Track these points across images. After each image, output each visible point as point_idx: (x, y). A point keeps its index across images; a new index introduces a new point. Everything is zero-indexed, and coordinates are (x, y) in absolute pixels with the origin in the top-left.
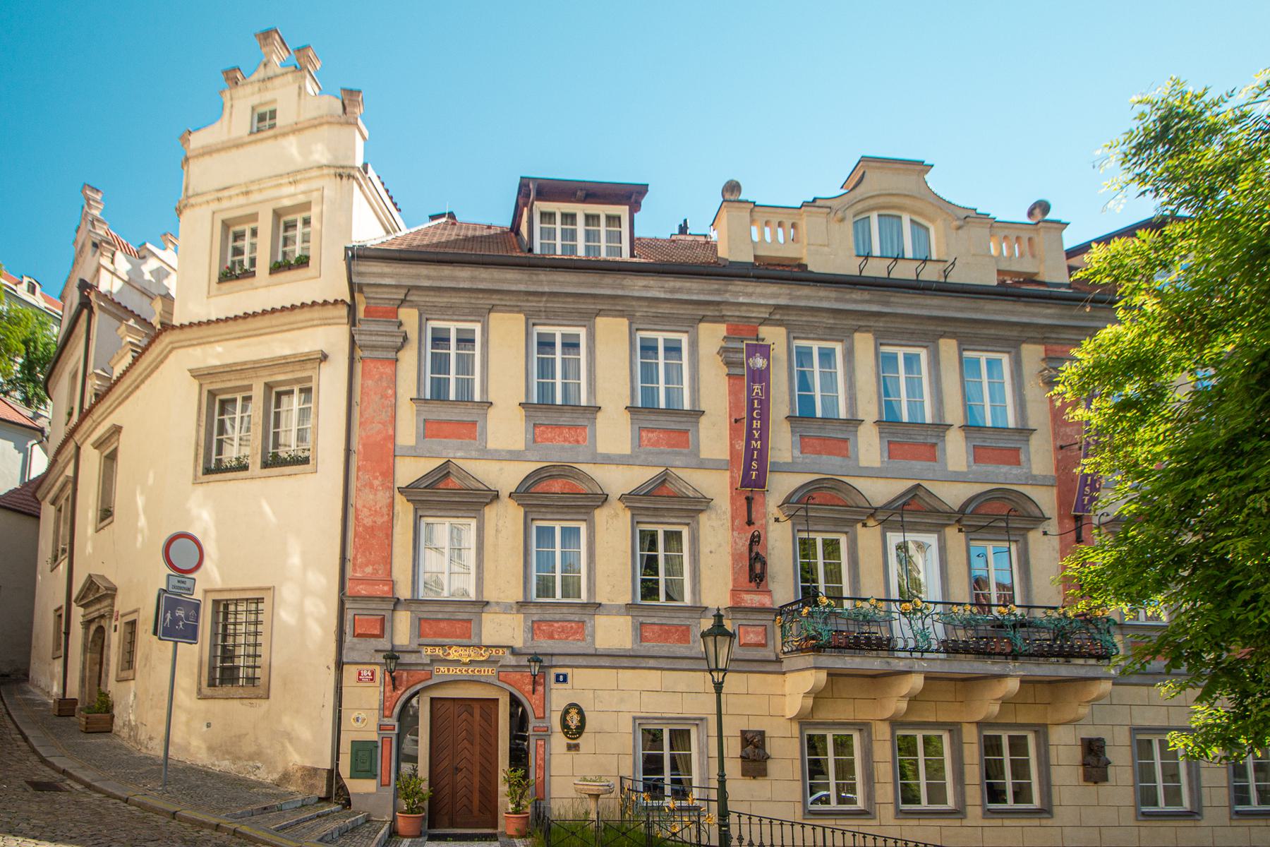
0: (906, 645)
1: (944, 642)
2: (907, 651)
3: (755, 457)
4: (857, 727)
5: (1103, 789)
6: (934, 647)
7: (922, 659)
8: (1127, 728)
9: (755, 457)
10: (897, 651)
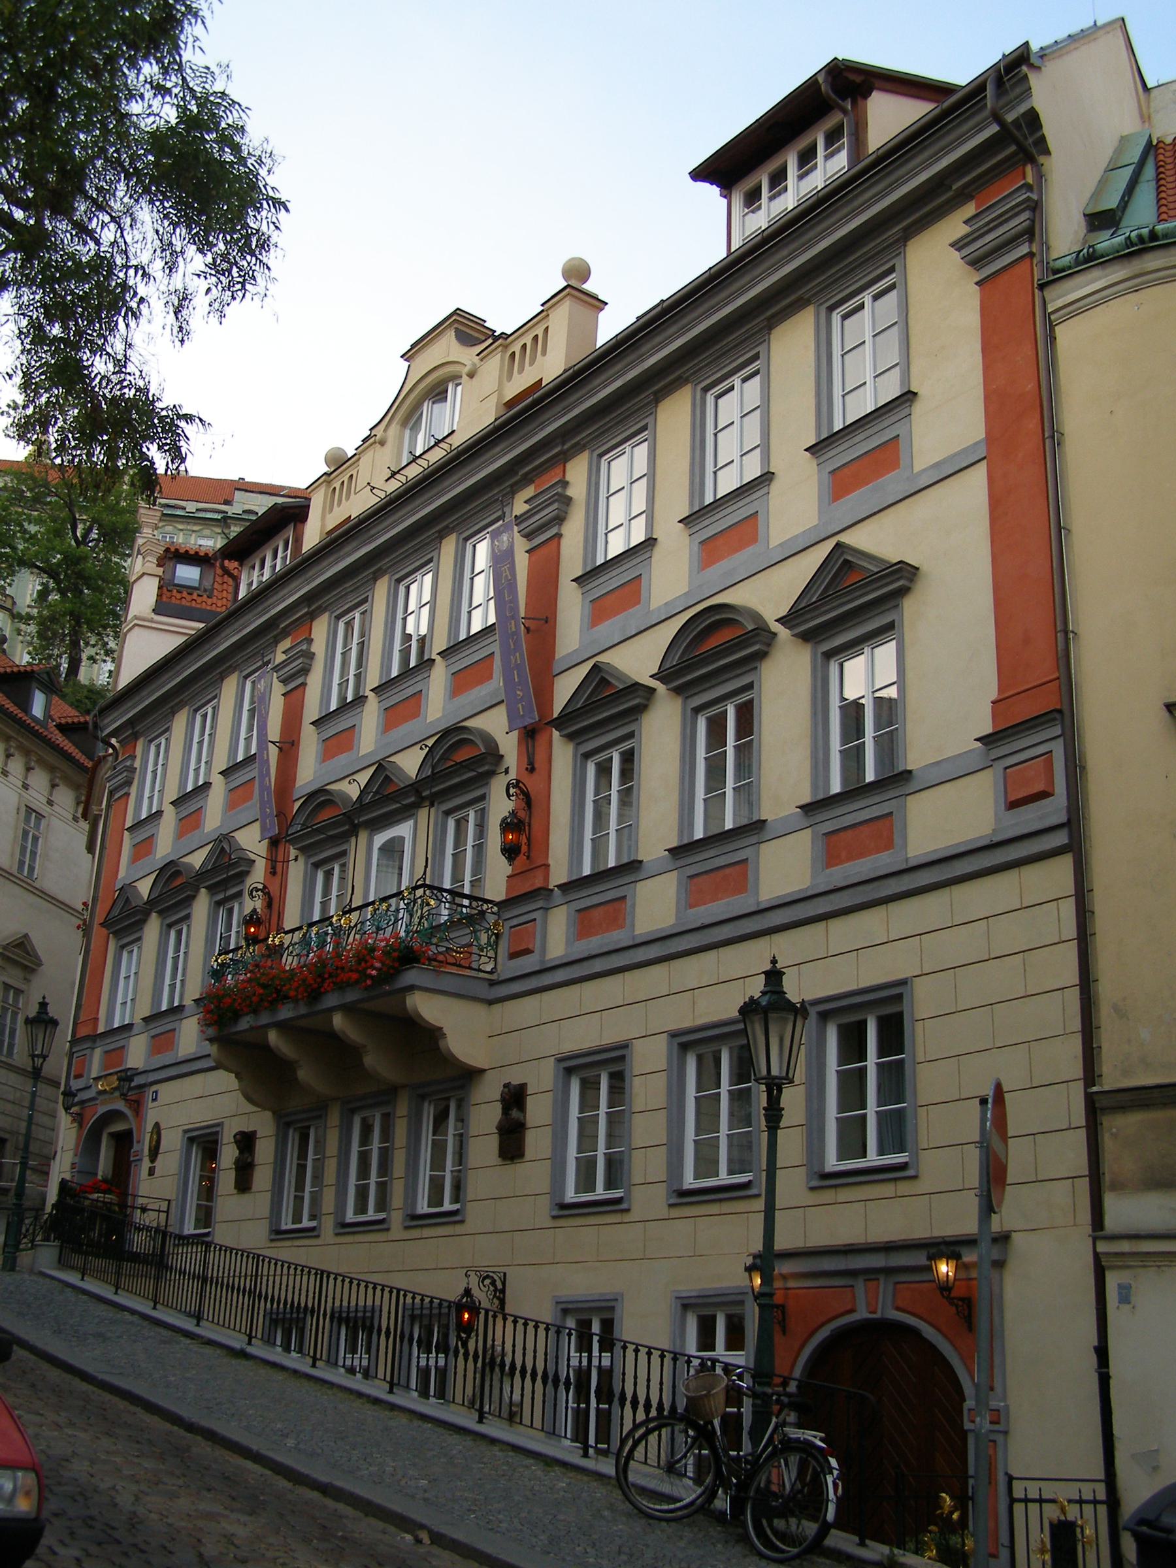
5: (520, 1169)
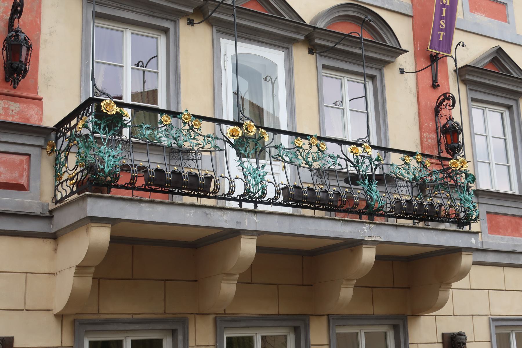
0: (232, 190)
1: (285, 189)
2: (235, 199)
3: (444, 15)
4: (168, 327)
6: (271, 194)
7: (255, 212)
8: (486, 318)
9: (444, 15)
10: (117, 187)
